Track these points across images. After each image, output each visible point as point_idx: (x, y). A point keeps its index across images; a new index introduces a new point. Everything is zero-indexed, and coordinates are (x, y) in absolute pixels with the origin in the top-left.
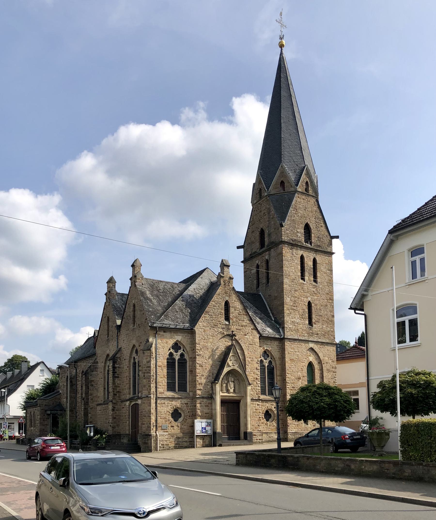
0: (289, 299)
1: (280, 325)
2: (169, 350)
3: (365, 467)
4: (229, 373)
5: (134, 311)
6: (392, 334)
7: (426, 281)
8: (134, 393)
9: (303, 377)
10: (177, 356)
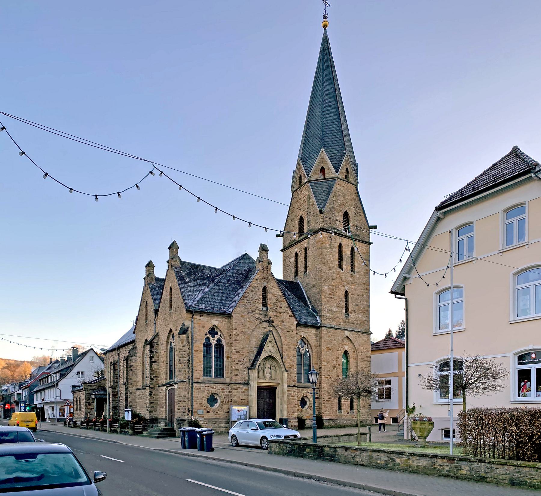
0: (326, 287)
1: (317, 312)
2: (206, 334)
3: (413, 461)
4: (266, 358)
5: (171, 295)
6: (434, 318)
7: (474, 262)
8: (171, 378)
9: (339, 365)
10: (213, 341)
